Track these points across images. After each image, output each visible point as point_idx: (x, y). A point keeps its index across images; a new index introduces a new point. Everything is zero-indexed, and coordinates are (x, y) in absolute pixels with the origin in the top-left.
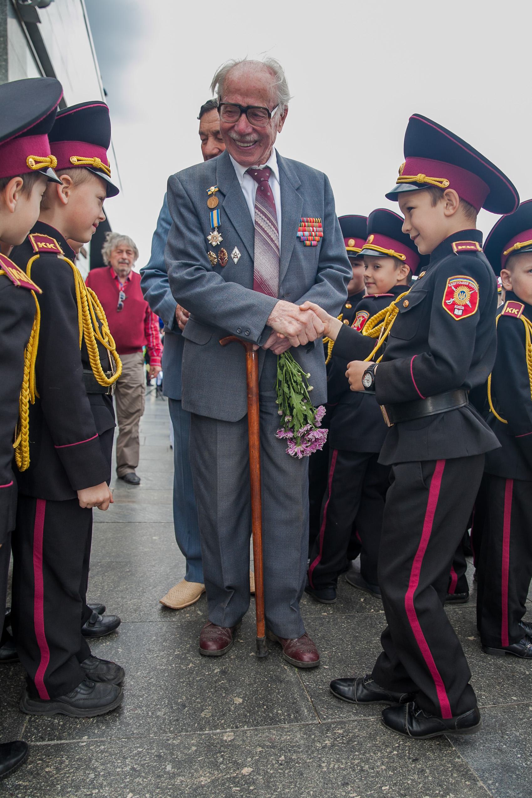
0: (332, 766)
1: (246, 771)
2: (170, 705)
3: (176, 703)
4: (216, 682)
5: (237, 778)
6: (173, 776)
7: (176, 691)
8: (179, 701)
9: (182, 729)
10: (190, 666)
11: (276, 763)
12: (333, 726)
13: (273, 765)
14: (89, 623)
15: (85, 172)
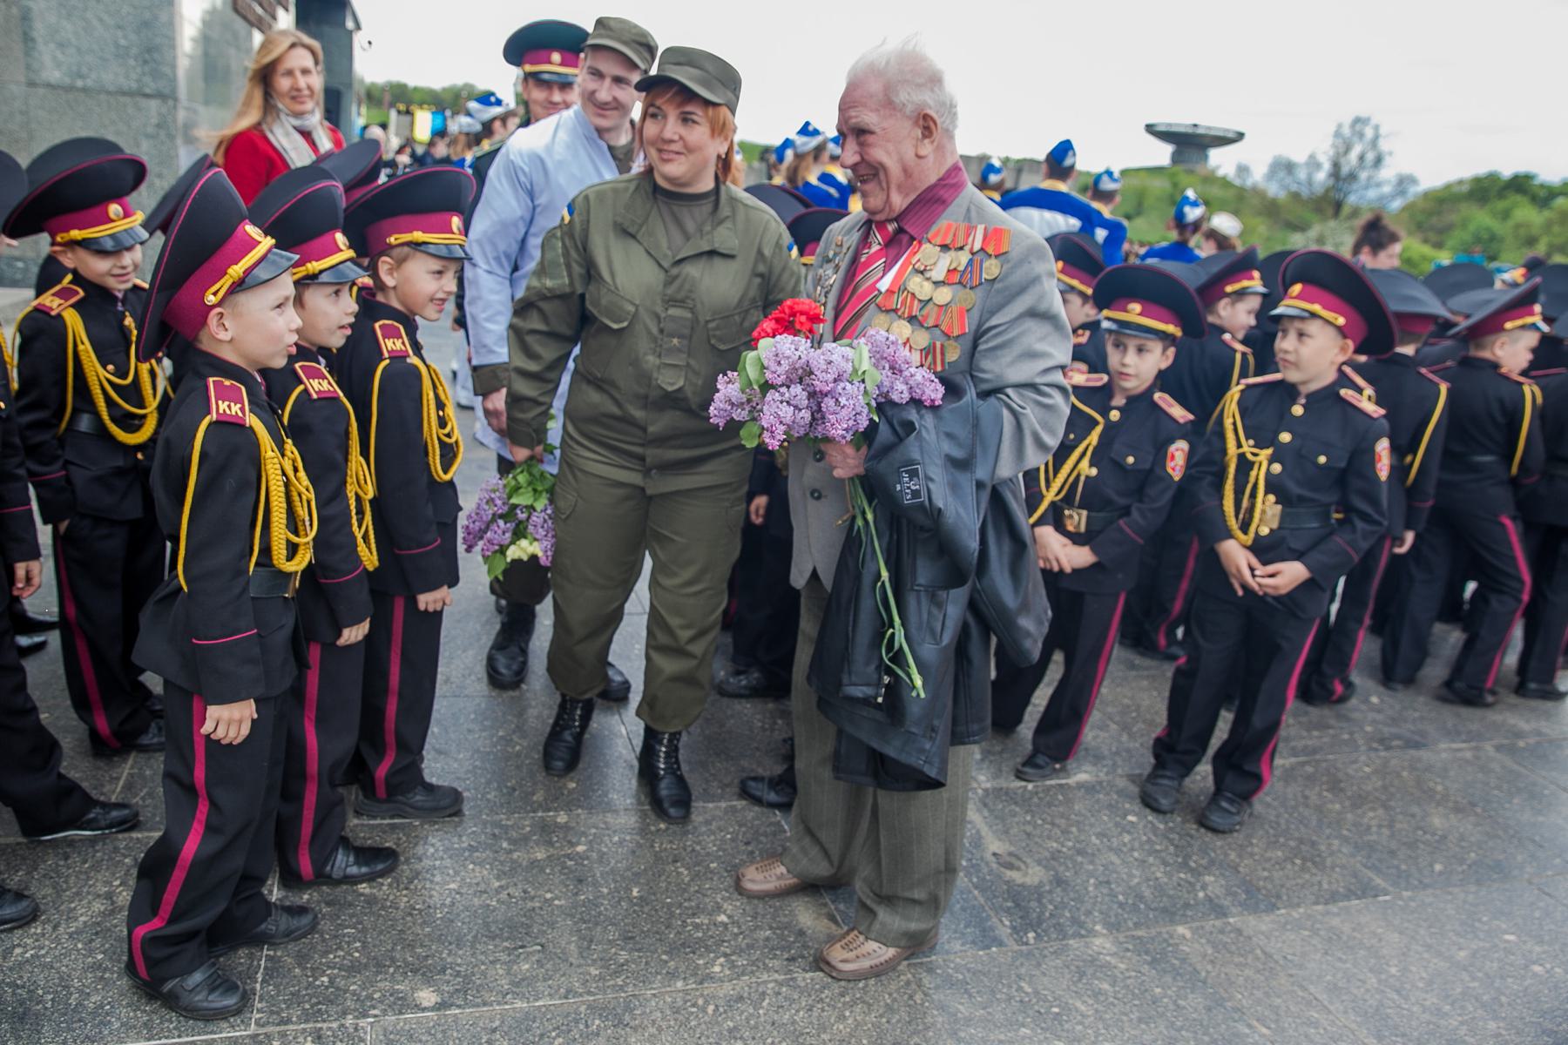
1: (580, 848)
2: (499, 789)
6: (511, 852)
14: (212, 165)
15: (406, 249)
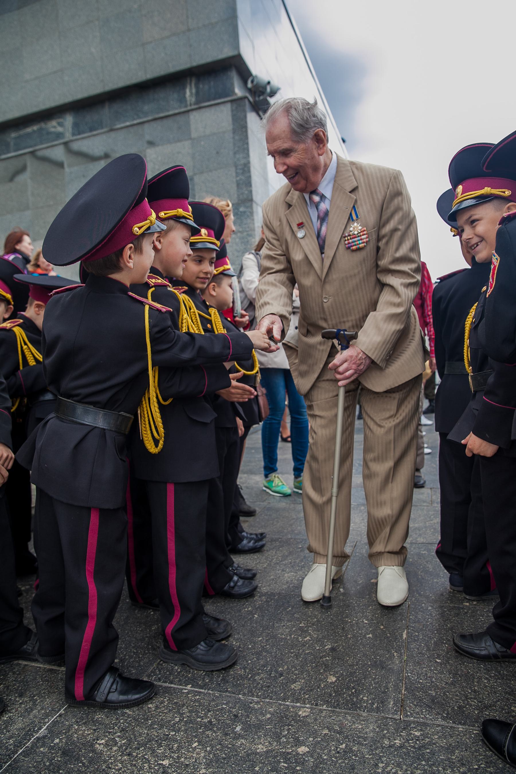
0: (389, 769)
3: (276, 671)
4: (321, 658)
5: (290, 754)
7: (282, 660)
8: (280, 669)
9: (268, 696)
10: (306, 639)
11: (334, 750)
12: (412, 725)
13: (330, 751)
